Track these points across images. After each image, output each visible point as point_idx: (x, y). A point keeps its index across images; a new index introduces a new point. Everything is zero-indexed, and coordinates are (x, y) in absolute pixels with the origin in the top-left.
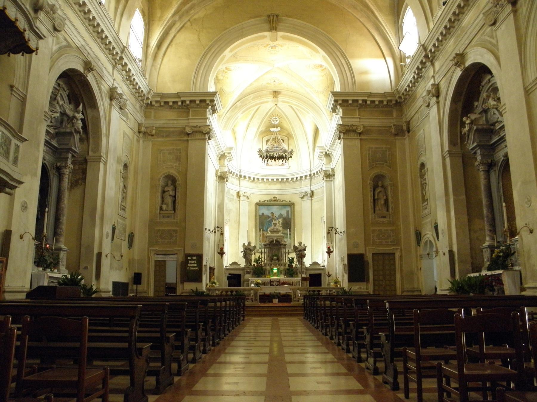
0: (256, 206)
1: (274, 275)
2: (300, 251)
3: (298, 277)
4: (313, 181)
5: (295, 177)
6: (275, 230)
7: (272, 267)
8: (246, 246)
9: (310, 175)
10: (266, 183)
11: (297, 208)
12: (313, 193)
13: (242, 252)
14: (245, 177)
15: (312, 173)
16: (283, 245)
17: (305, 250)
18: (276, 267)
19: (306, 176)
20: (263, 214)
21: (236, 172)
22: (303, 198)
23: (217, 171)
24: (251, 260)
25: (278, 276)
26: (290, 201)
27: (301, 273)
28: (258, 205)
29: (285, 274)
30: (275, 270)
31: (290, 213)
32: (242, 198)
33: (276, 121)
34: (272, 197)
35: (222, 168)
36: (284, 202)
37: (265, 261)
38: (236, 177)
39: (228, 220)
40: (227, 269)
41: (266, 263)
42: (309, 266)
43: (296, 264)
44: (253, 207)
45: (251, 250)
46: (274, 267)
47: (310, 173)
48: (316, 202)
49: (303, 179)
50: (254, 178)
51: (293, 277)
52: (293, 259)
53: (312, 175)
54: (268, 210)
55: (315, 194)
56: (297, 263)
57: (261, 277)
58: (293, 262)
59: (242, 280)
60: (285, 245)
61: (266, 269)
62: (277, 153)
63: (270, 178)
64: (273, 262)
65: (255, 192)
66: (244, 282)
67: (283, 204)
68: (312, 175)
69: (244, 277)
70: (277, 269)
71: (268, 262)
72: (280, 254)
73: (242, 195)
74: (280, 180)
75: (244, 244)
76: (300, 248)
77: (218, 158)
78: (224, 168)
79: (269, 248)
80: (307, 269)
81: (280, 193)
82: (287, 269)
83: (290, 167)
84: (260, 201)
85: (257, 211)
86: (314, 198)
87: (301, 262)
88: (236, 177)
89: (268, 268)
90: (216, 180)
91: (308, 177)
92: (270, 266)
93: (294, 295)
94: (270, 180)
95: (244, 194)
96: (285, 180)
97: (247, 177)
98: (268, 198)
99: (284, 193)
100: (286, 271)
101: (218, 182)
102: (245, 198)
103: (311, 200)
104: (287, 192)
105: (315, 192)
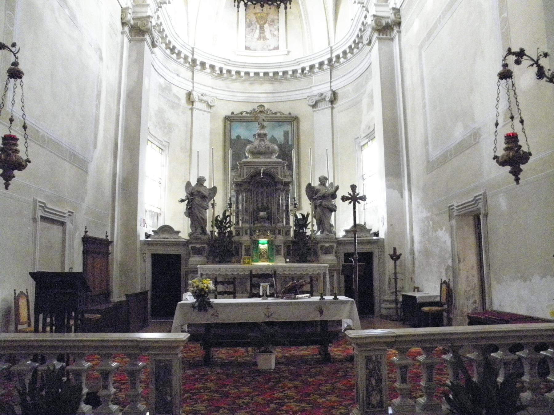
0: (225, 123)
1: (261, 256)
2: (324, 197)
3: (317, 261)
4: (335, 72)
6: (263, 149)
7: (255, 237)
8: (193, 189)
9: (330, 60)
11: (303, 126)
12: (334, 97)
13: (182, 201)
14: (203, 64)
15: (334, 55)
16: (281, 182)
17: (82, 383)
18: (265, 236)
19: (321, 64)
20: (238, 137)
21: (184, 52)
22: (314, 106)
24: (205, 221)
25: (270, 260)
26: (290, 114)
27: (327, 251)
28: (230, 120)
29: (287, 255)
30: (263, 244)
31: (290, 135)
32: (197, 105)
34: (256, 106)
35: (138, 9)
36: (278, 115)
37: (237, 223)
38: (185, 62)
39: (167, 144)
40: (147, 243)
41: (242, 228)
42: (344, 233)
43: (313, 231)
44: (220, 125)
45: (204, 197)
46: (259, 237)
47: (329, 56)
48: (342, 111)
49: (316, 70)
50: (221, 70)
51: (305, 261)
52: (305, 218)
53: (334, 59)
54: (248, 129)
55: (339, 96)
56: (316, 228)
57: (230, 262)
58: (306, 225)
59: (183, 270)
60: (287, 184)
61: (240, 243)
63: (252, 71)
64: (258, 225)
65: (223, 97)
66: (187, 273)
67: (278, 119)
68: (334, 59)
69: (187, 260)
70: (268, 243)
71: (246, 225)
72: (274, 208)
73: (197, 99)
74: (271, 74)
75: (189, 184)
76: (323, 191)
78: (144, 9)
79: (247, 190)
80: (339, 242)
82: (293, 242)
83: (289, 52)
84: (233, 113)
85: (227, 131)
87: (323, 224)
88: (185, 62)
89: (245, 239)
90: (123, 33)
91: (325, 67)
92: (251, 235)
93: (369, 377)
94: (252, 75)
95: (201, 97)
96: (281, 74)
97: (207, 66)
99: (279, 99)
100: (288, 247)
101: (130, 41)
102: (203, 106)
103: (332, 108)
104: (285, 96)
105: (340, 92)
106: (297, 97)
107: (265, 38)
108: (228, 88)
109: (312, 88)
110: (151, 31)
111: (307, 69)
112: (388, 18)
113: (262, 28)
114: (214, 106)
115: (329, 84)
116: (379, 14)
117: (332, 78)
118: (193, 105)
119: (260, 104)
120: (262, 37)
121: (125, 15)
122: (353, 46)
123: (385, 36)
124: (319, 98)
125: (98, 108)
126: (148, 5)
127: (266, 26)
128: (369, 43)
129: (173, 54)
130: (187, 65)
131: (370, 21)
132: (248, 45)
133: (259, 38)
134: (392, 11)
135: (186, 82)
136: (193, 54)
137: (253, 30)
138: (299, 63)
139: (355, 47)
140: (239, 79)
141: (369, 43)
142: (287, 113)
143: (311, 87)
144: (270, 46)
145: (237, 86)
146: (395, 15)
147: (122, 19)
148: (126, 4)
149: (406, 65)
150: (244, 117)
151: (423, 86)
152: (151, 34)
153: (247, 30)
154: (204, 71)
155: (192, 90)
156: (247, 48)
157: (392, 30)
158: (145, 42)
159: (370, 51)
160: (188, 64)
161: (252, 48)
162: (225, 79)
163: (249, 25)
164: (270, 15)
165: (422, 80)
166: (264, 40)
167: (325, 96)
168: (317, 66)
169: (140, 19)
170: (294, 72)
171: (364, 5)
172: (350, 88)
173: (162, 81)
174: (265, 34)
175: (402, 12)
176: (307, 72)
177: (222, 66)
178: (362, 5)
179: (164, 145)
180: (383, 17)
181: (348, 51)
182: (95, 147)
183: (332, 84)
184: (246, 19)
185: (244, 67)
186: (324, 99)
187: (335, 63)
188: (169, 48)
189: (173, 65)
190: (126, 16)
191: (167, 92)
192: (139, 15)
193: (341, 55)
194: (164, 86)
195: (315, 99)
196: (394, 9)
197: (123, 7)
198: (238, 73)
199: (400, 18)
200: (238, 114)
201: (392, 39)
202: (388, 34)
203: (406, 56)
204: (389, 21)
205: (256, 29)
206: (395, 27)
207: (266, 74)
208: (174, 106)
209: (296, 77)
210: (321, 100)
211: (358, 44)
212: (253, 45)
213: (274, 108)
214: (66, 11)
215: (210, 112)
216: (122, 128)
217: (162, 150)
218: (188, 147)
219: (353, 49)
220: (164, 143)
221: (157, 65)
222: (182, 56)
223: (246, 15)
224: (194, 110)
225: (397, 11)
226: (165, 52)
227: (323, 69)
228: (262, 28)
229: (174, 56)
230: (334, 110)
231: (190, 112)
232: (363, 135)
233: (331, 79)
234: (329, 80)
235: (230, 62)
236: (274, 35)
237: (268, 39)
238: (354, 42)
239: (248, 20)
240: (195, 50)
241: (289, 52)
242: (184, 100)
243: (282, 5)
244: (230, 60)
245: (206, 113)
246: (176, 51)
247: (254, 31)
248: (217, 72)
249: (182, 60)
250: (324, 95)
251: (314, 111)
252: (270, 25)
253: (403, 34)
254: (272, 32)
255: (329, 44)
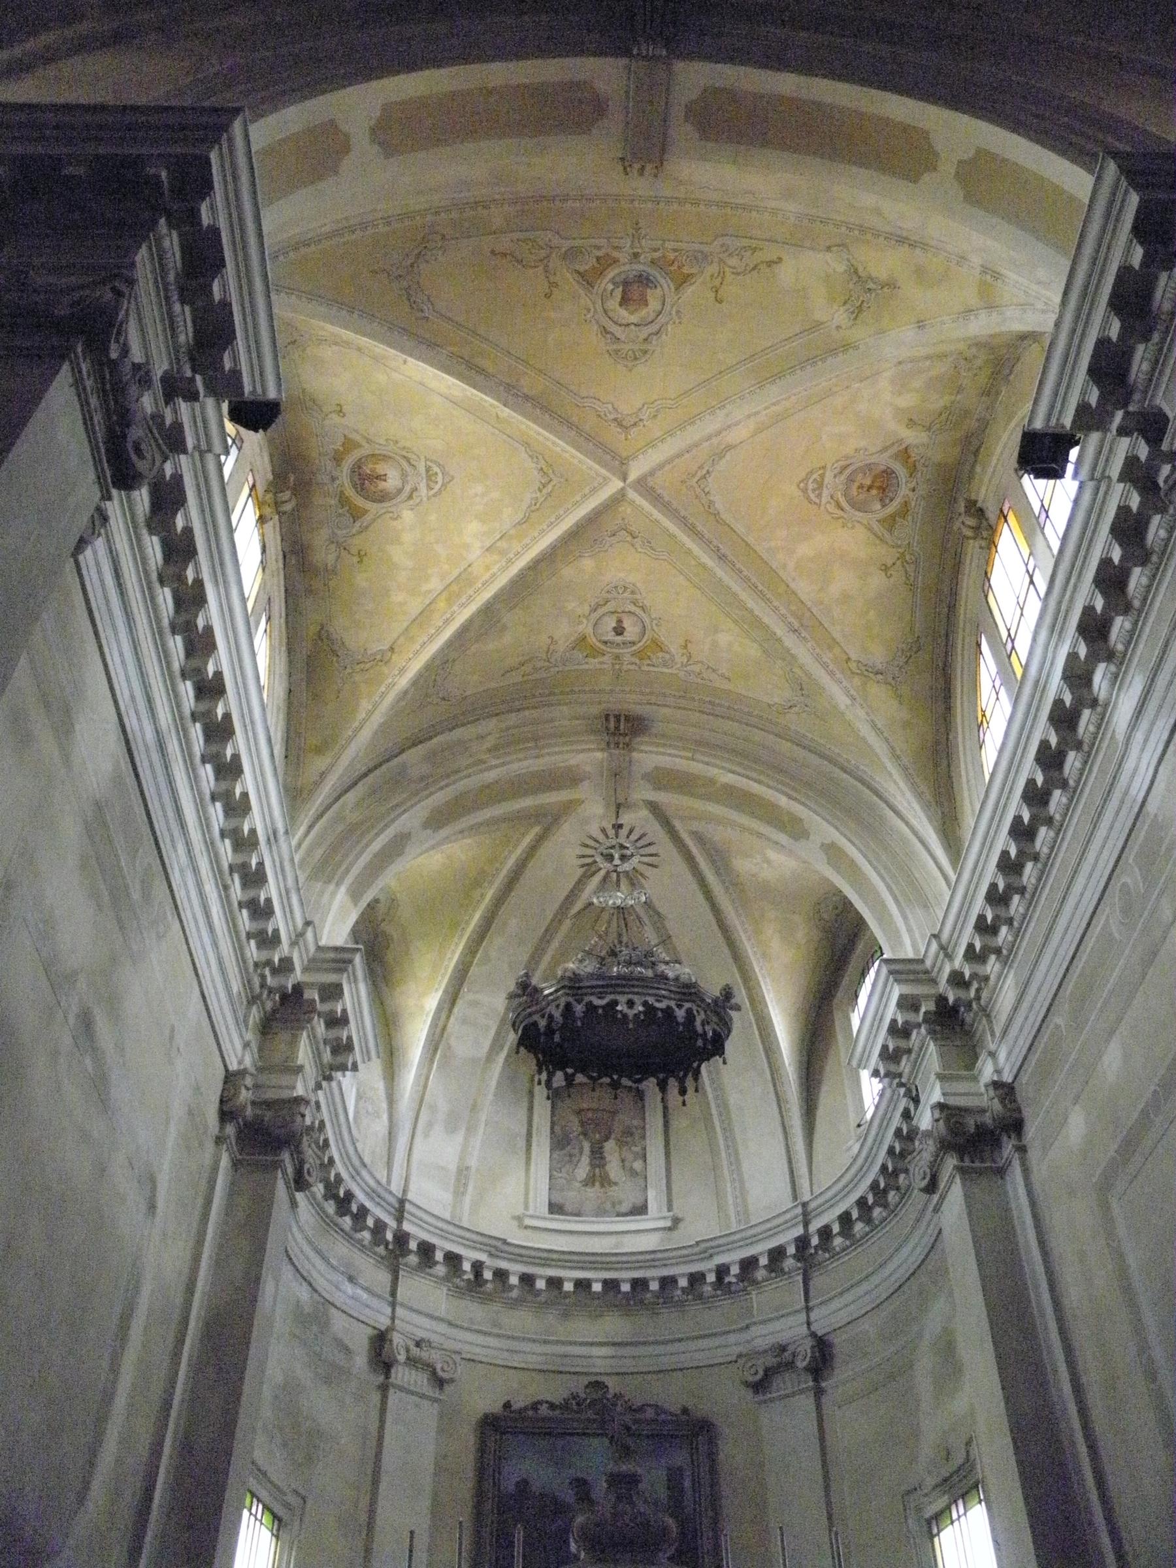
4: (819, 1281)
5: (707, 1267)
9: (802, 1243)
10: (546, 1304)
14: (426, 1250)
15: (815, 1226)
19: (777, 1254)
20: (523, 1485)
22: (759, 1386)
23: (231, 1078)
26: (685, 1411)
32: (402, 1375)
33: (623, 858)
34: (578, 1385)
35: (275, 1079)
36: (650, 1413)
44: (467, 1437)
47: (799, 1231)
49: (760, 1274)
50: (478, 1267)
53: (815, 1241)
62: (636, 998)
68: (815, 1241)
73: (402, 1358)
74: (626, 1287)
77: (255, 1014)
78: (285, 1080)
81: (628, 1365)
83: (676, 1221)
84: (507, 1405)
86: (840, 1381)
90: (219, 1140)
91: (789, 1263)
95: (415, 1351)
96: (654, 1286)
97: (439, 1256)
98: (555, 1391)
101: (236, 1164)
102: (417, 1379)
103: (819, 1393)
105: (839, 1341)
106: (701, 1358)
107: (606, 1181)
108: (496, 1324)
109: (753, 1329)
110: (300, 1143)
111: (735, 1270)
112: (983, 1111)
113: (598, 1155)
114: (452, 1381)
115: (802, 1317)
116: (953, 1101)
117: (812, 1294)
118: (387, 1375)
119: (593, 1379)
120: (598, 1177)
121: (232, 1091)
122: (870, 1200)
123: (977, 1164)
124: (775, 1361)
125: (115, 1369)
126: (299, 1069)
127: (610, 1145)
128: (931, 1187)
129: (342, 1215)
130: (381, 1250)
131: (925, 1120)
132: (558, 1198)
133: (589, 1181)
134: (992, 1093)
135: (375, 1303)
136: (400, 1219)
137: (571, 1156)
138: (711, 1251)
139: (875, 1203)
140: (530, 1298)
141: (931, 1187)
142: (676, 1408)
143: (747, 1327)
144: (620, 1203)
145: (522, 1320)
146: (1002, 1101)
147: (221, 1101)
148: (240, 1063)
149: (1060, 1245)
150: (543, 1419)
151: (1132, 1304)
152: (297, 1151)
153: (555, 1156)
154: (428, 1270)
155: (391, 1329)
156: (555, 1208)
157: (997, 1144)
158: (279, 1172)
159: (936, 1210)
160: (382, 1247)
161: (569, 1207)
162: (487, 1298)
163: (560, 1142)
164: (620, 1116)
165: (1127, 1289)
166: (602, 1186)
167: (794, 1355)
168: (764, 1261)
169: (269, 1104)
170: (696, 1279)
171: (903, 1080)
172: (866, 1325)
173: (304, 1294)
174: (607, 1168)
175: (1021, 1094)
176: (734, 1280)
177: (483, 1257)
178: (897, 1080)
179: (287, 1506)
180: (966, 1110)
181: (855, 1214)
182: (81, 1498)
183: (813, 1316)
184: (553, 1124)
185: (546, 1263)
186: (790, 1365)
187: (816, 1253)
188: (335, 1197)
189: (341, 1249)
190: (236, 1094)
191: (315, 1328)
192: (271, 1095)
193: (836, 1228)
194: (307, 1310)
195: (761, 1363)
196: (997, 1085)
197: (230, 1068)
198: (527, 1280)
199: (1019, 1110)
200: (526, 1409)
201: (1001, 1172)
202: (987, 1155)
203: (1056, 1219)
204: (987, 1119)
205: (581, 1153)
206: (1005, 1138)
207: (611, 1285)
208: (333, 1375)
209: (700, 1297)
210: (779, 1365)
211: (885, 1191)
212: (570, 1197)
213: (635, 1392)
214: (88, 1061)
215: (436, 1400)
216: (175, 1439)
217: (280, 1520)
218: (363, 1518)
219: (870, 1209)
220: (292, 1499)
221: (298, 1243)
222: (370, 1222)
223: (553, 1114)
224: (391, 1391)
225: (1005, 1090)
226: (322, 1209)
227: (782, 1270)
228: (598, 1155)
229: (347, 1221)
230: (824, 1399)
231: (376, 1397)
232: (930, 1481)
233: (807, 1300)
234: (803, 1303)
235: (506, 1248)
236: (633, 1173)
237: (616, 1184)
238: (874, 1186)
239: (557, 1129)
240: (408, 1206)
241: (676, 1221)
242: (361, 1360)
243: (673, 1084)
244: (505, 1242)
245: (426, 1403)
246: (354, 1208)
247: (575, 1160)
248: (465, 1277)
249: (366, 1235)
250: (791, 1348)
251: (760, 1403)
252: (621, 1143)
253: (1033, 1155)
254: (627, 1164)
255: (795, 1198)
